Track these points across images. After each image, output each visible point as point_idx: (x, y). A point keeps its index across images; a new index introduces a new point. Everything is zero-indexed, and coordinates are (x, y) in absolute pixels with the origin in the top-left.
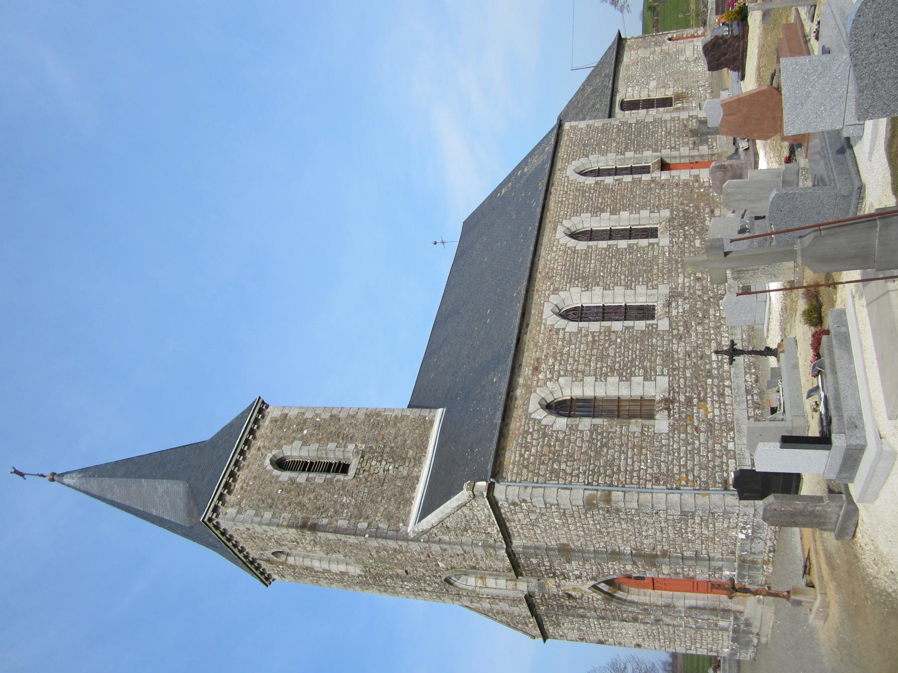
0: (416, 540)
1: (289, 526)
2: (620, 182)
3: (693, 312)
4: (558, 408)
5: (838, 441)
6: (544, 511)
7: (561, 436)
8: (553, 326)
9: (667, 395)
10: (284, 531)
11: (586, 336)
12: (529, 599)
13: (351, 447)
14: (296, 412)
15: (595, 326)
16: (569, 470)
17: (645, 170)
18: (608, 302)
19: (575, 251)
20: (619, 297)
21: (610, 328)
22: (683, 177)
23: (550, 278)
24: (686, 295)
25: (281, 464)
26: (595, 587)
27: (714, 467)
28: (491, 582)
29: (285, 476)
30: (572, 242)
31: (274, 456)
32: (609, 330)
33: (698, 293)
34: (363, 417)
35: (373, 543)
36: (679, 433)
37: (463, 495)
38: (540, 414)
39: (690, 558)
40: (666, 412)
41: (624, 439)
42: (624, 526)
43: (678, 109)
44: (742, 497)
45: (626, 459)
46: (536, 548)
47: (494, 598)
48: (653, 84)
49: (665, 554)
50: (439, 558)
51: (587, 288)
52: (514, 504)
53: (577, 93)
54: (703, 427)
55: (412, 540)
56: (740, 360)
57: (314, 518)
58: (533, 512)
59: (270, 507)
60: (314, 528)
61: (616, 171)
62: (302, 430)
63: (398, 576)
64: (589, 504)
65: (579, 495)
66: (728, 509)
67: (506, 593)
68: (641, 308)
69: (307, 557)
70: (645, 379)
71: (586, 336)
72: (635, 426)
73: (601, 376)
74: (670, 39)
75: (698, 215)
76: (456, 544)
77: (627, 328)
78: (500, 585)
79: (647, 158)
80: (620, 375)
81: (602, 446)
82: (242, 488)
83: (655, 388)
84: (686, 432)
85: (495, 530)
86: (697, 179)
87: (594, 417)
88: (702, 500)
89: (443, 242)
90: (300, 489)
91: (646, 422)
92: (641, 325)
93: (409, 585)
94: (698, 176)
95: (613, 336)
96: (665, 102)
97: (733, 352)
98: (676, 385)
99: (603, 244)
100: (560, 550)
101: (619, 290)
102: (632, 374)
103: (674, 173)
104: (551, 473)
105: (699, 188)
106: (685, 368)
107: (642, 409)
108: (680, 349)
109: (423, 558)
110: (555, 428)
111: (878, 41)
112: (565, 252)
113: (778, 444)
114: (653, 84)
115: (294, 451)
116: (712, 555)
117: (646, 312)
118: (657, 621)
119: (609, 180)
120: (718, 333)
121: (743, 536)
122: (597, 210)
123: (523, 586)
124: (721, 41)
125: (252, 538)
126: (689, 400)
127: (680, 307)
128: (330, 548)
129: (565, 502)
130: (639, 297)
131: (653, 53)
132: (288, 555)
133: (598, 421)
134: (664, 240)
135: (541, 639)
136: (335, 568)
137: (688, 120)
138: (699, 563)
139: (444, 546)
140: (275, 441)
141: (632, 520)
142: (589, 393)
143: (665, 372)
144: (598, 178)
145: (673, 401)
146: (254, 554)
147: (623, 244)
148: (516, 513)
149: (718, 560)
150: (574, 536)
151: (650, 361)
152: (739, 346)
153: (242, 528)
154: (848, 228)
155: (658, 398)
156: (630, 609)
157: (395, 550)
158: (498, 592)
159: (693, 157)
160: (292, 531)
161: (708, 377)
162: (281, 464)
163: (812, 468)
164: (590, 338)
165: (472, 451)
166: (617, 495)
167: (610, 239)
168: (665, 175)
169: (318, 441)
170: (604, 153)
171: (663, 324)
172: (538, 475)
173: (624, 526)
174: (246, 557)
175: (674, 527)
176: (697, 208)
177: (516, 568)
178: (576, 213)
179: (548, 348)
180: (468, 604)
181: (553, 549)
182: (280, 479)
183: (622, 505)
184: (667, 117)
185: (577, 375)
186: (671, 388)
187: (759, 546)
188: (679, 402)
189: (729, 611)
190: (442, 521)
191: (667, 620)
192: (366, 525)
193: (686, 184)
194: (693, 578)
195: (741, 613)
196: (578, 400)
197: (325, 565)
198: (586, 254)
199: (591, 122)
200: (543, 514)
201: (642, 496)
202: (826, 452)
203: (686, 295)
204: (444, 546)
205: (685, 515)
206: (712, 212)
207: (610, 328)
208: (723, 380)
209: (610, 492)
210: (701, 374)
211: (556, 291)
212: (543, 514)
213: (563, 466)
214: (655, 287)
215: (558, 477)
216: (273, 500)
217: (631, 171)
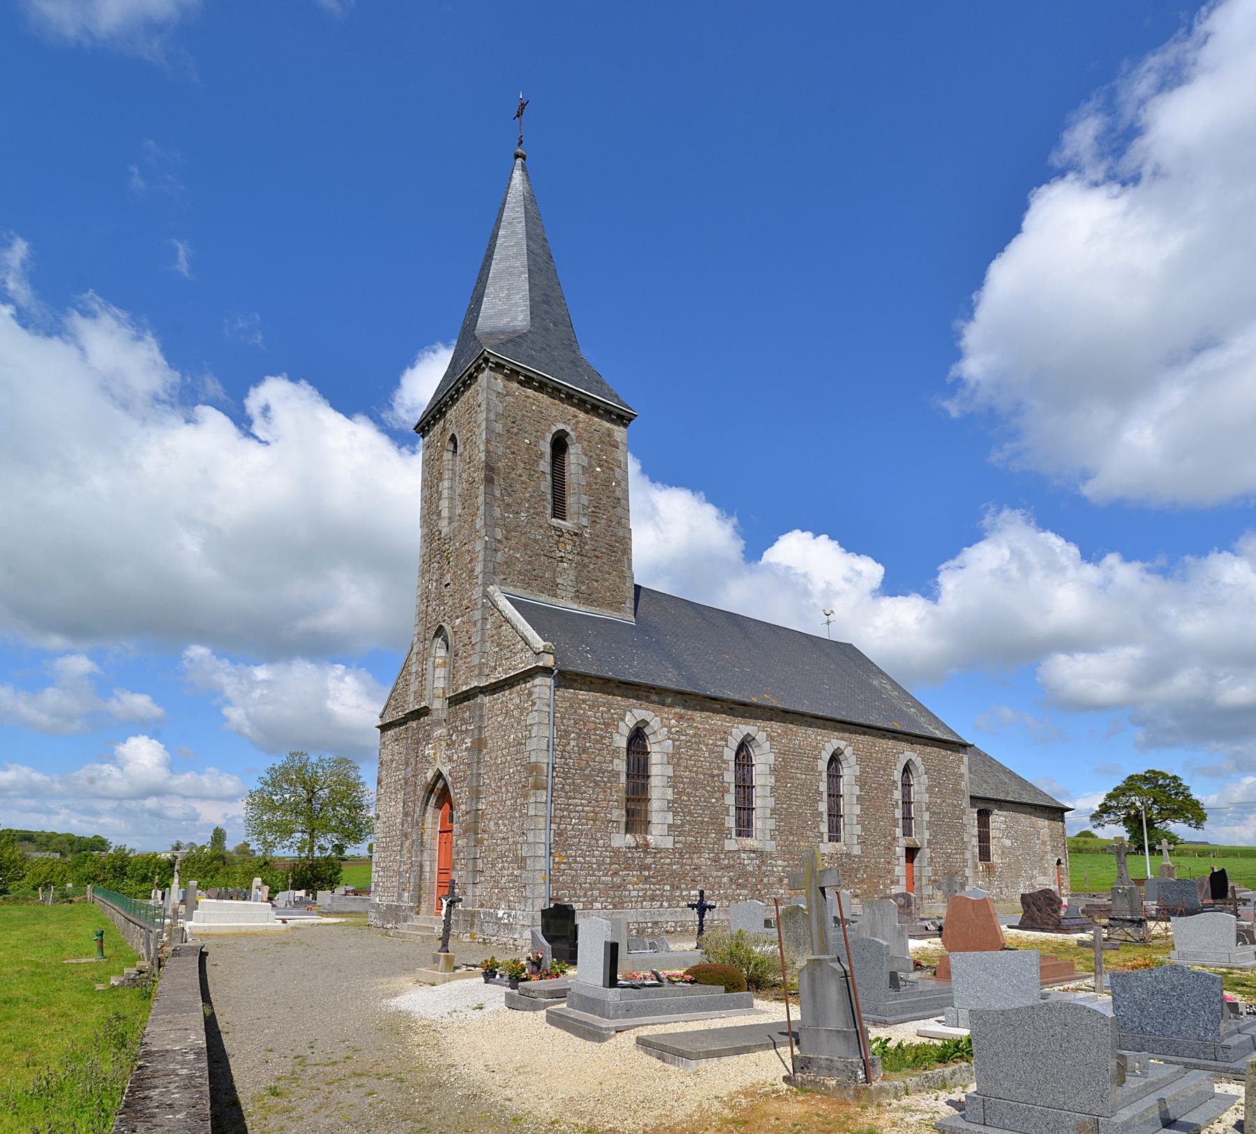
0: (486, 595)
1: (487, 452)
2: (895, 806)
3: (744, 874)
4: (638, 736)
5: (613, 994)
6: (523, 723)
7: (606, 741)
8: (731, 734)
9: (653, 845)
10: (482, 448)
11: (719, 768)
12: (424, 712)
13: (584, 521)
14: (621, 459)
15: (730, 777)
16: (568, 748)
17: (907, 832)
18: (757, 792)
19: (816, 758)
20: (762, 801)
21: (728, 792)
22: (897, 868)
23: (786, 733)
24: (764, 868)
25: (560, 444)
26: (439, 776)
27: (575, 889)
28: (441, 672)
29: (546, 447)
30: (826, 756)
31: (568, 434)
32: (725, 791)
33: (765, 880)
34: (621, 534)
35: (479, 546)
36: (611, 857)
37: (538, 642)
38: (630, 721)
39: (475, 865)
40: (633, 845)
41: (605, 804)
42: (508, 803)
43: (976, 867)
44: (544, 913)
45: (582, 805)
46: (481, 716)
47: (422, 675)
48: (1008, 843)
49: (479, 842)
50: (465, 619)
51: (774, 770)
52: (530, 694)
53: (1001, 765)
54: (617, 880)
55: (485, 590)
56: (694, 915)
57: (498, 480)
58: (521, 714)
59: (508, 431)
60: (489, 481)
61: (907, 803)
62: (600, 466)
63: (442, 575)
64: (533, 768)
65: (543, 759)
66: (530, 901)
67: (429, 687)
68: (749, 823)
69: (454, 474)
70: (670, 826)
71: (719, 768)
72: (619, 814)
73: (673, 782)
74: (1059, 862)
75: (853, 882)
76: (483, 635)
77: (727, 809)
78: (439, 681)
79: (921, 833)
80: (674, 801)
81: (595, 781)
82: (528, 397)
83: (658, 836)
84: (611, 864)
85: (500, 675)
86: (895, 882)
87: (628, 775)
88: (539, 877)
89: (828, 623)
90: (533, 462)
91: (623, 825)
92: (731, 822)
93: (433, 586)
94: (898, 882)
95: (718, 795)
96: (985, 854)
97: (702, 908)
98: (663, 855)
99: (823, 787)
100: (480, 739)
101: (771, 802)
102: (675, 814)
103: (903, 860)
104: (565, 731)
105: (884, 884)
106: (683, 865)
107: (636, 820)
108: (704, 860)
109: (464, 602)
110: (615, 735)
111: (1058, 1029)
112: (816, 748)
113: (609, 940)
114: (1008, 843)
115: (574, 457)
116: (479, 886)
117: (744, 828)
118: (406, 835)
119: (898, 795)
120: (720, 898)
121: (500, 915)
122: (861, 781)
123: (438, 705)
124: (1055, 907)
125: (470, 409)
126: (648, 868)
127: (750, 863)
128: (467, 498)
129: (532, 745)
130: (761, 822)
131: (1044, 843)
132: (455, 452)
133: (623, 778)
134: (827, 848)
135: (380, 723)
136: (444, 504)
137: (963, 875)
138: (471, 875)
139: (479, 625)
140: (585, 435)
141: (515, 810)
142: (655, 770)
143: (678, 845)
144: (900, 784)
145: (645, 852)
146: (451, 414)
147: (823, 807)
148: (519, 695)
149: (474, 892)
150: (496, 752)
151: (690, 831)
152: (708, 915)
153: (480, 398)
154: (856, 995)
155: (649, 837)
156: (418, 809)
157: (473, 571)
158: (429, 677)
159: (920, 879)
160: (483, 456)
161: (672, 886)
162: (560, 444)
163: (587, 970)
164: (716, 772)
165: (587, 652)
166: (543, 796)
167: (829, 795)
168: (900, 851)
169: (589, 484)
170: (929, 789)
171: (731, 844)
172: (562, 718)
173: (508, 803)
174: (446, 404)
175: (510, 850)
176: (862, 881)
177: (457, 700)
178: (860, 760)
179: (705, 729)
180: (415, 650)
181: (480, 733)
182: (541, 442)
183: (532, 800)
184: (968, 855)
185: (674, 758)
186: (659, 850)
187: (490, 929)
188: (645, 858)
189: (420, 902)
190: (507, 621)
191: (407, 843)
192: (499, 538)
193: (890, 872)
194: (454, 868)
195: (418, 913)
196: (646, 760)
197: (445, 494)
198: (812, 769)
199: (966, 777)
200: (519, 723)
201: (542, 819)
202: (601, 983)
203: (764, 868)
204: (479, 625)
205: (521, 862)
206: (856, 896)
207: (728, 792)
208: (668, 900)
209: (546, 788)
210: (677, 880)
211: (770, 738)
212: (519, 723)
213: (573, 743)
214: (773, 838)
215: (561, 737)
216: (517, 434)
217: (907, 818)
